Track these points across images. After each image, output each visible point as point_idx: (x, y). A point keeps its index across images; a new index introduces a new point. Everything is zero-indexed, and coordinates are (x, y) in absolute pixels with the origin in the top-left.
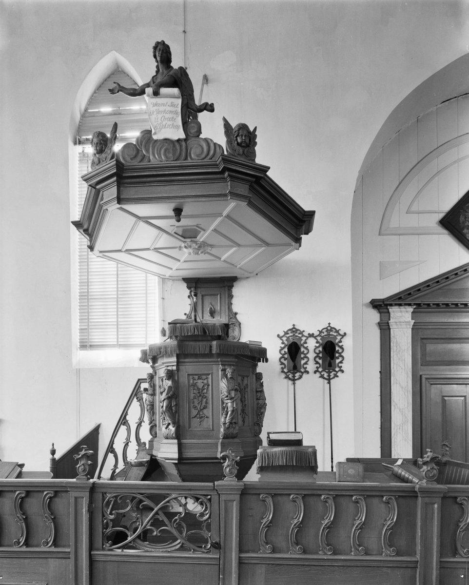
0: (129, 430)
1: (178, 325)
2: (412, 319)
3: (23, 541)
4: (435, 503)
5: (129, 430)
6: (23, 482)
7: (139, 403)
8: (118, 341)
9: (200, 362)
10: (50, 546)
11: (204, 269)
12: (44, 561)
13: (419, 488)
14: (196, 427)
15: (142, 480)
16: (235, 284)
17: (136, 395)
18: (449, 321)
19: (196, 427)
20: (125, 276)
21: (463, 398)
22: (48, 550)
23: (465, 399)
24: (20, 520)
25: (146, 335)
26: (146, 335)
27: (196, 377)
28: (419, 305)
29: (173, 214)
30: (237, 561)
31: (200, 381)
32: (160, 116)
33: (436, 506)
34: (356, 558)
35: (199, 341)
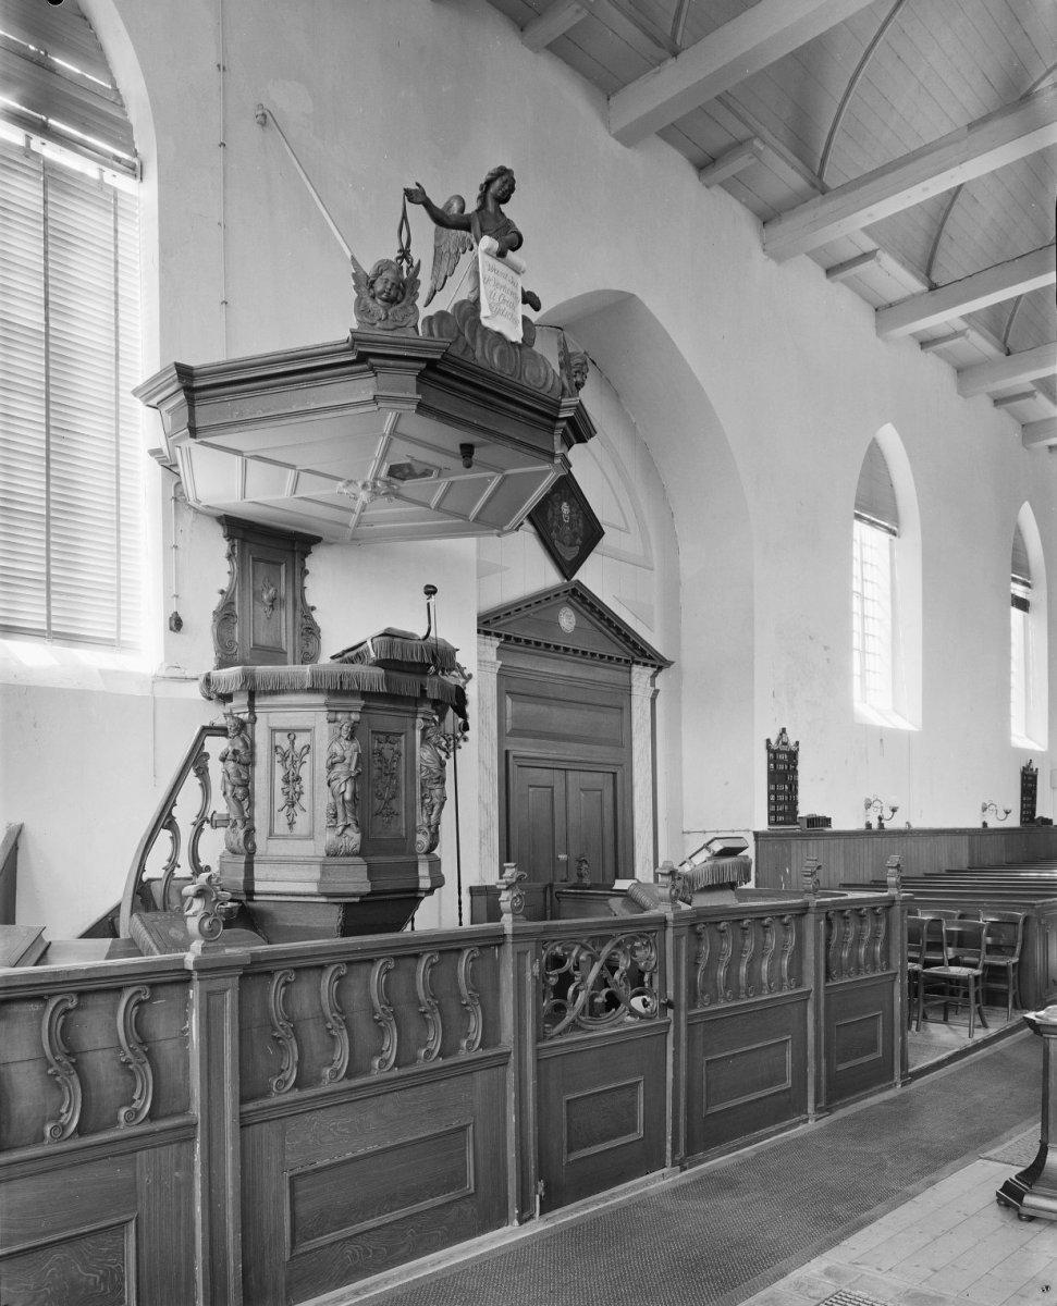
0: (176, 839)
1: (396, 640)
2: (498, 659)
3: (479, 1038)
4: (226, 990)
5: (176, 839)
6: (484, 931)
7: (198, 781)
8: (49, 624)
9: (399, 710)
10: (342, 1080)
11: (291, 512)
12: (468, 1078)
13: (195, 963)
14: (380, 833)
15: (109, 957)
16: (313, 548)
17: (195, 763)
18: (515, 665)
19: (380, 833)
20: (69, 469)
21: (599, 793)
22: (433, 1066)
23: (553, 790)
24: (340, 1024)
25: (119, 621)
26: (119, 621)
27: (382, 737)
28: (508, 638)
29: (458, 450)
30: (237, 1120)
31: (387, 746)
32: (499, 292)
33: (822, 923)
34: (791, 993)
35: (404, 671)
